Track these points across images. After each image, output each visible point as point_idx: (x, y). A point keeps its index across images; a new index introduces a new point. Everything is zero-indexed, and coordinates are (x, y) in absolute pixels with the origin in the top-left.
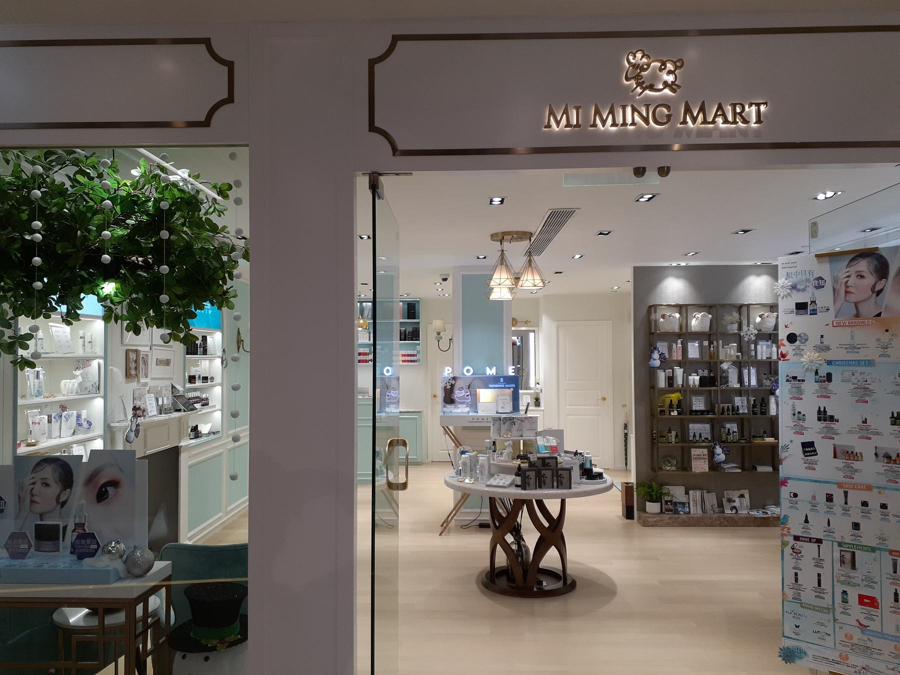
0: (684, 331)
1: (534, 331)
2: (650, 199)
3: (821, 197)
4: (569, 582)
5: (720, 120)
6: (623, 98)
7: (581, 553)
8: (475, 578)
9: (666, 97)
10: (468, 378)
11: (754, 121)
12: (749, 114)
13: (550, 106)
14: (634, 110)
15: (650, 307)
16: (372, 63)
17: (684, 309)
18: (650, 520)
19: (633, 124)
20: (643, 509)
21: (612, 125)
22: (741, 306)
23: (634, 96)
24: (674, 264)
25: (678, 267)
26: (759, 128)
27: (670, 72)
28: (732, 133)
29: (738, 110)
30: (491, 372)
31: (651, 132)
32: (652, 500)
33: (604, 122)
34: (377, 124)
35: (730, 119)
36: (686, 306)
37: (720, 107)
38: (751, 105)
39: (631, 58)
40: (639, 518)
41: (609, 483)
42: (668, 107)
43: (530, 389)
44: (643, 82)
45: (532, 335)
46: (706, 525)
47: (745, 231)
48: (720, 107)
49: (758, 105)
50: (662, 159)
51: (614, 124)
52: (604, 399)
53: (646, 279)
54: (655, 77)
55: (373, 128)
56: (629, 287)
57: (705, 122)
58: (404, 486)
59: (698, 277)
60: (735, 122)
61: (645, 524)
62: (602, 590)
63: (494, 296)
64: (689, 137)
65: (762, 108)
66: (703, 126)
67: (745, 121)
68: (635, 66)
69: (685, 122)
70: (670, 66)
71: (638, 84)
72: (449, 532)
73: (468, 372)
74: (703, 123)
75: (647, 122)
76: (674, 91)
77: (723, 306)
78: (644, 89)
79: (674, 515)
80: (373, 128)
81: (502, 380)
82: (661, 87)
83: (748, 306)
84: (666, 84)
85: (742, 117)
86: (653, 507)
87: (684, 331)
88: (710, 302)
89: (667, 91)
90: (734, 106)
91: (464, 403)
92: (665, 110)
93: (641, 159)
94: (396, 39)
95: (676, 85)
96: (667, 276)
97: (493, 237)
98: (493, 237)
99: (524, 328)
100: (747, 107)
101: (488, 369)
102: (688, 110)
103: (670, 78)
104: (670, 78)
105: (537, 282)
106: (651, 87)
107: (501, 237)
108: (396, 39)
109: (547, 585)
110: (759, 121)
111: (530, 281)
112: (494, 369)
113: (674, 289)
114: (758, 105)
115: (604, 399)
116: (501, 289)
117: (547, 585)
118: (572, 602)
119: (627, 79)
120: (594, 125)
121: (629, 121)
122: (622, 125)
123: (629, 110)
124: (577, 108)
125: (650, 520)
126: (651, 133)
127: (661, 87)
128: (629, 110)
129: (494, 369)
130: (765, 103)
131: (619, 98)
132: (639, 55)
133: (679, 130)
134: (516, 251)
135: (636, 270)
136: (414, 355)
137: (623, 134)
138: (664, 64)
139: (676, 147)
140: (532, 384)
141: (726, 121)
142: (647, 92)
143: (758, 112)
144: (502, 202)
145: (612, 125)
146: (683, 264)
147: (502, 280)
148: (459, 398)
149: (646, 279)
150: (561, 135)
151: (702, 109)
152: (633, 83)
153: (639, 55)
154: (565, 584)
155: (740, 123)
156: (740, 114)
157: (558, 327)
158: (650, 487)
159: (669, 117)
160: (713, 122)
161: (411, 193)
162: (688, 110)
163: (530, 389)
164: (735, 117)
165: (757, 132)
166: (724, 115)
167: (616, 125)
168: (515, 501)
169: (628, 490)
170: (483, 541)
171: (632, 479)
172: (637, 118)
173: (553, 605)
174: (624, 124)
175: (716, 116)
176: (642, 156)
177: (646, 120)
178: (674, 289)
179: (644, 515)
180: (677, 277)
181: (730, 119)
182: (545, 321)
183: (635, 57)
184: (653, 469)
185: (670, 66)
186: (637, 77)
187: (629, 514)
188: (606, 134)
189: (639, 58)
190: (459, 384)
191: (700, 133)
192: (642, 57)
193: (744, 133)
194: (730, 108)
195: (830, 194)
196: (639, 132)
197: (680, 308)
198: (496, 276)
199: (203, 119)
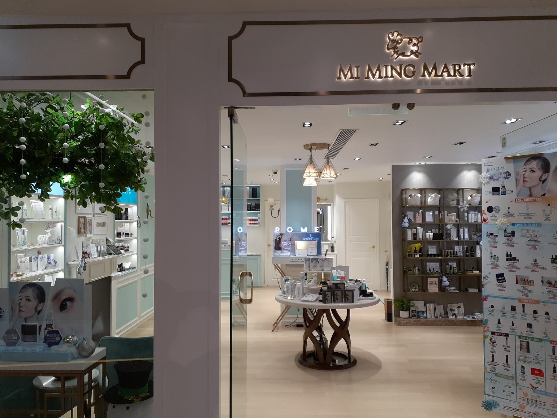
0: (423, 205)
1: (330, 205)
2: (402, 123)
3: (508, 122)
4: (352, 360)
5: (445, 74)
6: (386, 61)
7: (360, 343)
8: (294, 358)
9: (412, 60)
10: (290, 234)
11: (467, 75)
12: (464, 70)
13: (341, 66)
14: (392, 68)
15: (402, 190)
16: (230, 39)
17: (423, 192)
18: (402, 322)
19: (392, 76)
20: (398, 315)
21: (379, 78)
22: (459, 190)
23: (392, 60)
24: (417, 164)
25: (420, 166)
26: (470, 79)
27: (414, 45)
28: (453, 82)
29: (457, 68)
30: (304, 230)
31: (403, 82)
32: (403, 310)
33: (374, 76)
34: (234, 77)
35: (452, 73)
36: (425, 189)
37: (446, 66)
38: (464, 65)
39: (390, 36)
40: (396, 321)
41: (377, 299)
42: (413, 67)
43: (328, 241)
44: (398, 51)
45: (329, 207)
46: (437, 325)
47: (461, 143)
48: (446, 66)
49: (469, 65)
50: (410, 98)
51: (380, 77)
52: (374, 247)
53: (400, 172)
54: (405, 47)
55: (231, 79)
56: (390, 178)
57: (436, 75)
58: (250, 301)
59: (432, 171)
60: (455, 76)
61: (399, 324)
62: (372, 365)
63: (306, 183)
64: (426, 85)
65: (472, 67)
66: (435, 78)
67: (461, 75)
68: (393, 41)
69: (424, 76)
70: (414, 41)
71: (395, 52)
72: (278, 329)
73: (290, 230)
74: (435, 76)
75: (401, 76)
76: (417, 56)
77: (448, 189)
78: (399, 55)
79: (417, 319)
80: (231, 79)
81: (311, 235)
82: (409, 54)
83: (463, 189)
84: (412, 52)
85: (459, 73)
86: (404, 314)
87: (423, 205)
88: (440, 187)
89: (413, 56)
90: (454, 66)
91: (287, 249)
92: (412, 68)
93: (397, 99)
94: (245, 24)
95: (419, 53)
96: (413, 171)
97: (305, 147)
98: (305, 147)
99: (324, 203)
100: (462, 66)
101: (302, 228)
102: (426, 68)
103: (415, 49)
104: (415, 49)
105: (332, 175)
106: (403, 54)
107: (310, 147)
108: (245, 24)
109: (339, 362)
110: (470, 75)
111: (328, 174)
112: (306, 228)
113: (417, 179)
114: (469, 65)
115: (374, 247)
116: (310, 179)
117: (339, 362)
118: (354, 373)
119: (388, 49)
120: (368, 77)
121: (389, 75)
122: (385, 77)
123: (389, 68)
124: (357, 67)
125: (402, 322)
126: (403, 82)
127: (409, 54)
128: (389, 68)
129: (306, 228)
130: (474, 64)
131: (383, 61)
132: (395, 34)
133: (420, 81)
134: (320, 155)
135: (394, 167)
136: (256, 220)
137: (386, 83)
138: (411, 39)
139: (418, 91)
140: (329, 238)
141: (449, 75)
142: (401, 57)
143: (469, 70)
144: (311, 125)
145: (379, 78)
146: (423, 164)
147: (311, 174)
148: (284, 246)
149: (400, 172)
150: (347, 83)
151: (435, 68)
152: (392, 51)
153: (395, 34)
154: (350, 362)
155: (458, 76)
156: (458, 70)
157: (345, 202)
158: (402, 302)
159: (414, 72)
160: (442, 75)
161: (254, 119)
162: (426, 68)
163: (328, 241)
164: (455, 73)
165: (468, 82)
166: (448, 71)
167: (381, 78)
168: (319, 310)
169: (389, 303)
170: (299, 335)
171: (391, 297)
172: (394, 73)
173: (342, 375)
174: (386, 77)
175: (443, 72)
176: (397, 96)
177: (400, 74)
178: (417, 179)
179: (398, 319)
180: (419, 171)
181: (452, 73)
182: (337, 199)
183: (393, 35)
184: (404, 291)
185: (414, 41)
186: (394, 48)
187: (389, 318)
188: (375, 83)
189: (395, 36)
190: (284, 238)
191: (433, 82)
192: (398, 35)
193: (460, 82)
194: (452, 67)
195: (513, 120)
196: (396, 82)
197: (421, 191)
198: (307, 171)
199: (126, 74)
